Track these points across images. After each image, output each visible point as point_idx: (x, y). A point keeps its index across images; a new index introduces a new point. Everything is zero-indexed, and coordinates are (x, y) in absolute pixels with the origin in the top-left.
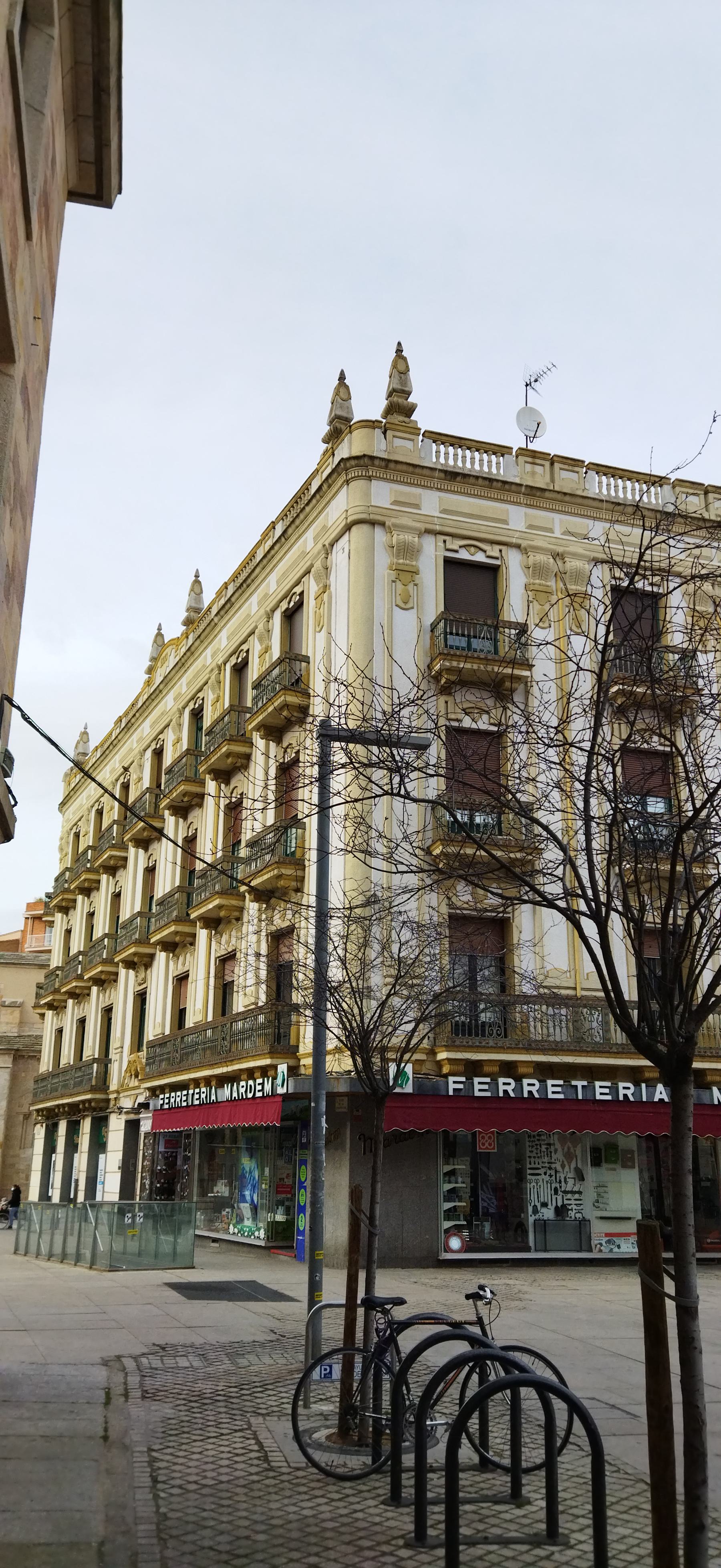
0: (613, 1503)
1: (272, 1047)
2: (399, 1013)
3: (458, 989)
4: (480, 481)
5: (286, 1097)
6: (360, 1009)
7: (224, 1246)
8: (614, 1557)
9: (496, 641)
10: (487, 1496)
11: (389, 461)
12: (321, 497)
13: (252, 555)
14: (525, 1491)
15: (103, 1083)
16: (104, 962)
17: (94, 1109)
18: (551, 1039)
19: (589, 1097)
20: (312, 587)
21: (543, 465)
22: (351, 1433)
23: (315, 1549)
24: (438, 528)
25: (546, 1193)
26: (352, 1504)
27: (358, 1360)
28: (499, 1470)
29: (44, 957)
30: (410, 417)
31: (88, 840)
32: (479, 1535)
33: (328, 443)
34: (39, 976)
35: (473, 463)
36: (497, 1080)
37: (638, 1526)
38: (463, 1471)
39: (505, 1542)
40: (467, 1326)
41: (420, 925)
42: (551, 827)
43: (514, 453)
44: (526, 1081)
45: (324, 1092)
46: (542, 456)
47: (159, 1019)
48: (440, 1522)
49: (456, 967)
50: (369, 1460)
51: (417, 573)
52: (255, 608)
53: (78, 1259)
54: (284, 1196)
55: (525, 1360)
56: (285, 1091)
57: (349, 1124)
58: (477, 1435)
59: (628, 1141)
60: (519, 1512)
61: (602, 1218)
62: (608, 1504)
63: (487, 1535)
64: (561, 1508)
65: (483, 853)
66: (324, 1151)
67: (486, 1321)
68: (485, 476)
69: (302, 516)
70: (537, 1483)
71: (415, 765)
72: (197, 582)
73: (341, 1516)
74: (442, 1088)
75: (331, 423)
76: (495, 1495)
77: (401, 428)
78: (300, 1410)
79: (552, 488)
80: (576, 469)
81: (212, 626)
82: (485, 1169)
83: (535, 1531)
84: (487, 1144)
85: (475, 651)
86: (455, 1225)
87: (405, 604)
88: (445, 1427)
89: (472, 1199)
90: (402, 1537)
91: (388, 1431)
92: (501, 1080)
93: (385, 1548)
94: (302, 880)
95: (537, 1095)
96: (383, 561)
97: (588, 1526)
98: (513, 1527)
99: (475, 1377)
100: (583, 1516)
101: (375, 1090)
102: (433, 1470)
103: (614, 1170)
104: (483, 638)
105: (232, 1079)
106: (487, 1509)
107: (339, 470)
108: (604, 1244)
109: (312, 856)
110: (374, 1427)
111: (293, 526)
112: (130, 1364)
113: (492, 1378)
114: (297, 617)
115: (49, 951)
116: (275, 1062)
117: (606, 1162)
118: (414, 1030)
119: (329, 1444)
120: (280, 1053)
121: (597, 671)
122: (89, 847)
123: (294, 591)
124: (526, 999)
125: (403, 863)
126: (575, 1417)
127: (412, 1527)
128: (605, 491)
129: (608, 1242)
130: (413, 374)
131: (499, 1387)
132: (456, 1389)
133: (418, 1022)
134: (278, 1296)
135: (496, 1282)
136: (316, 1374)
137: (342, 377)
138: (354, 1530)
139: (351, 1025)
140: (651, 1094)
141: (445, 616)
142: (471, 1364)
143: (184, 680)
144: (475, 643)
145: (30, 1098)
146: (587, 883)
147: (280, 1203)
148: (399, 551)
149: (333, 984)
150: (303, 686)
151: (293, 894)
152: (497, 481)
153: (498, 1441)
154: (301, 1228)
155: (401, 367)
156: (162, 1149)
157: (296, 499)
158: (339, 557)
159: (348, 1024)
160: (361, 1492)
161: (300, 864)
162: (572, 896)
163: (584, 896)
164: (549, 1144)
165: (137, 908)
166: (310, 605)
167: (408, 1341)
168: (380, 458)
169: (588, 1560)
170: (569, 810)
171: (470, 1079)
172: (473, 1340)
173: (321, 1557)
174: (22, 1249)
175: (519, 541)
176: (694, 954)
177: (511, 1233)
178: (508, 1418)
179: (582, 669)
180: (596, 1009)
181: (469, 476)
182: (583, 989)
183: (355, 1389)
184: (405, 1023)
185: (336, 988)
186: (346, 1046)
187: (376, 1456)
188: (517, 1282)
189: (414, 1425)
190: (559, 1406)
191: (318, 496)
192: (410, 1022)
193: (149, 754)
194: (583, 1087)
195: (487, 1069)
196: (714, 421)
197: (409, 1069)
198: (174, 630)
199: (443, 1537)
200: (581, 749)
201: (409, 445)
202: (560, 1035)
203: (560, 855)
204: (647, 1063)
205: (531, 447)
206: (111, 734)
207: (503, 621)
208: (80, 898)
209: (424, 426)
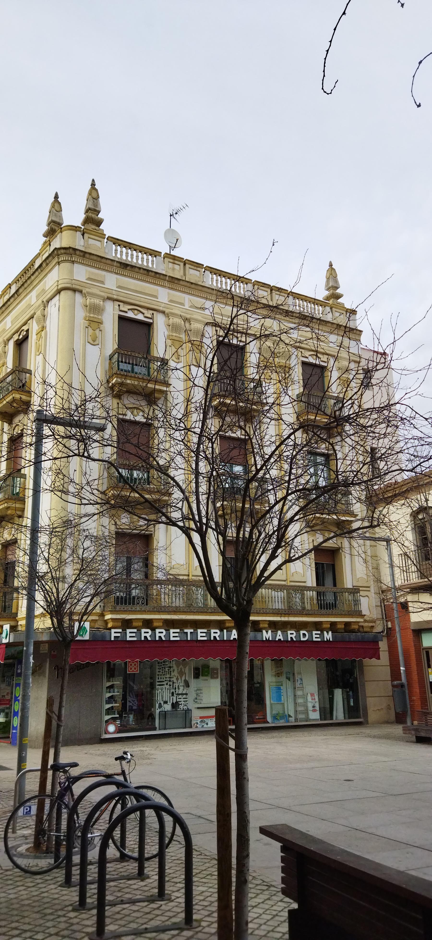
0: (197, 874)
2: (81, 591)
3: (118, 576)
4: (142, 271)
6: (57, 589)
8: (196, 904)
9: (149, 368)
10: (124, 876)
11: (85, 253)
12: (42, 271)
14: (146, 871)
18: (174, 605)
19: (194, 639)
20: (34, 327)
21: (179, 265)
22: (42, 846)
23: (16, 918)
24: (115, 297)
25: (166, 695)
26: (40, 888)
27: (48, 802)
28: (132, 860)
30: (99, 226)
32: (118, 899)
33: (47, 237)
35: (137, 259)
36: (140, 631)
37: (211, 885)
38: (110, 862)
39: (133, 902)
40: (115, 776)
41: (96, 537)
42: (176, 478)
43: (162, 256)
44: (157, 631)
45: (32, 641)
46: (179, 259)
48: (94, 894)
49: (118, 562)
50: (52, 861)
51: (101, 323)
54: (5, 706)
55: (149, 793)
56: (7, 641)
57: (48, 660)
58: (119, 840)
59: (215, 663)
60: (142, 883)
61: (198, 708)
62: (194, 874)
63: (123, 899)
64: (167, 879)
65: (137, 495)
66: (31, 677)
67: (127, 772)
68: (144, 268)
69: (29, 282)
70: (154, 866)
71: (95, 438)
73: (34, 896)
75: (49, 224)
76: (128, 875)
77: (93, 233)
78: (10, 835)
79: (184, 279)
80: (199, 269)
82: (131, 683)
83: (151, 894)
84: (133, 669)
85: (136, 373)
86: (112, 718)
87: (94, 342)
88: (100, 837)
89: (123, 702)
90: (71, 905)
91: (64, 843)
92: (143, 630)
93: (60, 913)
94: (23, 510)
95: (164, 639)
96: (80, 314)
97: (182, 888)
98: (138, 892)
99: (119, 806)
100: (180, 883)
101: (64, 638)
102: (91, 863)
103: (207, 680)
104: (141, 366)
106: (123, 883)
107: (54, 255)
108: (199, 723)
109: (29, 493)
110: (56, 841)
111: (23, 288)
113: (129, 805)
114: (24, 345)
117: (202, 676)
118: (90, 601)
119: (28, 853)
120: (5, 618)
121: (205, 387)
123: (23, 328)
124: (160, 582)
125: (85, 499)
126: (177, 825)
127: (77, 899)
128: (215, 284)
129: (201, 722)
130: (101, 200)
131: (133, 810)
132: (107, 814)
133: (93, 596)
135: (134, 750)
136: (21, 812)
138: (42, 904)
139: (51, 599)
140: (229, 636)
141: (118, 351)
142: (117, 799)
144: (136, 369)
146: (195, 512)
148: (90, 308)
149: (40, 574)
150: (27, 389)
151: (16, 518)
152: (152, 271)
153: (132, 843)
154: (15, 726)
155: (94, 195)
157: (26, 270)
158: (53, 309)
159: (49, 599)
160: (47, 880)
161: (23, 501)
162: (187, 519)
163: (194, 519)
164: (170, 667)
166: (33, 338)
167: (78, 788)
168: (80, 251)
169: (182, 907)
170: (186, 469)
171: (124, 630)
172: (118, 785)
173: (19, 923)
175: (164, 309)
176: (254, 551)
177: (146, 720)
178: (138, 829)
179: (196, 386)
180: (200, 587)
181: (135, 267)
182: (193, 576)
183: (44, 819)
184: (85, 597)
185: (42, 577)
186: (47, 612)
187: (57, 858)
188: (148, 749)
189: (80, 838)
190: (168, 820)
191: (39, 270)
192: (88, 596)
194: (191, 633)
195: (135, 624)
196: (273, 245)
197: (87, 625)
199: (96, 903)
200: (195, 433)
201: (98, 244)
202: (179, 602)
203: (181, 496)
204: (227, 618)
205: (172, 253)
207: (154, 357)
209: (108, 233)
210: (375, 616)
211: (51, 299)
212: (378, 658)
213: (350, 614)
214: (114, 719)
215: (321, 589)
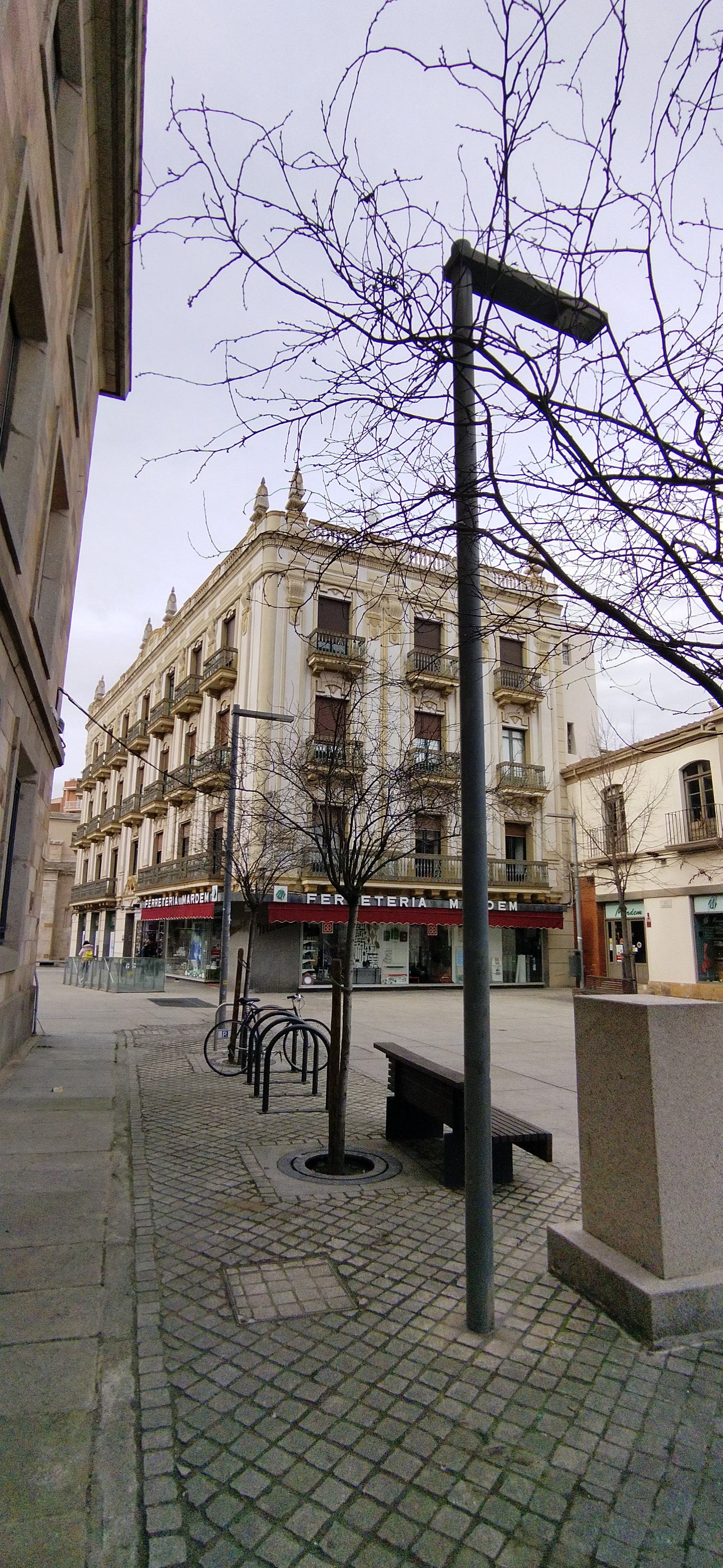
1: (210, 875)
5: (216, 903)
7: (182, 982)
13: (206, 584)
15: (112, 893)
16: (113, 822)
17: (107, 907)
20: (240, 608)
29: (76, 815)
31: (103, 749)
34: (74, 828)
47: (145, 857)
52: (207, 616)
53: (100, 987)
69: (236, 564)
72: (173, 595)
74: (304, 898)
75: (255, 509)
81: (181, 624)
92: (336, 896)
105: (187, 892)
112: (128, 1033)
114: (232, 623)
115: (80, 812)
116: (211, 884)
122: (104, 753)
134: (208, 1005)
137: (263, 482)
143: (163, 655)
145: (69, 899)
147: (214, 960)
156: (147, 930)
158: (257, 592)
165: (133, 792)
166: (239, 618)
174: (68, 982)
193: (141, 698)
198: (158, 623)
206: (118, 684)
208: (98, 782)
210: (562, 890)
211: (256, 581)
212: (562, 928)
213: (537, 886)
214: (311, 973)
215: (511, 861)
